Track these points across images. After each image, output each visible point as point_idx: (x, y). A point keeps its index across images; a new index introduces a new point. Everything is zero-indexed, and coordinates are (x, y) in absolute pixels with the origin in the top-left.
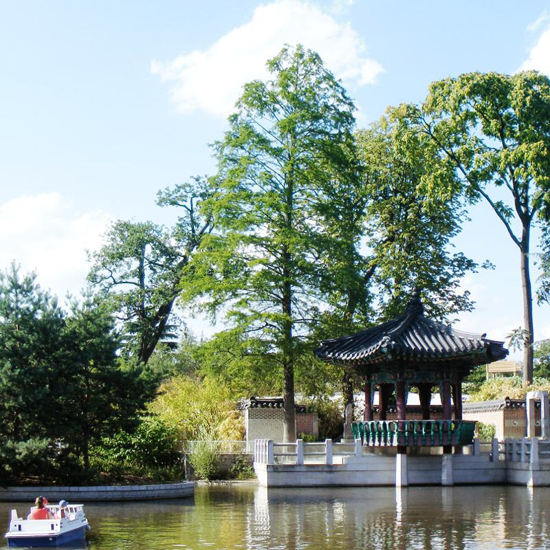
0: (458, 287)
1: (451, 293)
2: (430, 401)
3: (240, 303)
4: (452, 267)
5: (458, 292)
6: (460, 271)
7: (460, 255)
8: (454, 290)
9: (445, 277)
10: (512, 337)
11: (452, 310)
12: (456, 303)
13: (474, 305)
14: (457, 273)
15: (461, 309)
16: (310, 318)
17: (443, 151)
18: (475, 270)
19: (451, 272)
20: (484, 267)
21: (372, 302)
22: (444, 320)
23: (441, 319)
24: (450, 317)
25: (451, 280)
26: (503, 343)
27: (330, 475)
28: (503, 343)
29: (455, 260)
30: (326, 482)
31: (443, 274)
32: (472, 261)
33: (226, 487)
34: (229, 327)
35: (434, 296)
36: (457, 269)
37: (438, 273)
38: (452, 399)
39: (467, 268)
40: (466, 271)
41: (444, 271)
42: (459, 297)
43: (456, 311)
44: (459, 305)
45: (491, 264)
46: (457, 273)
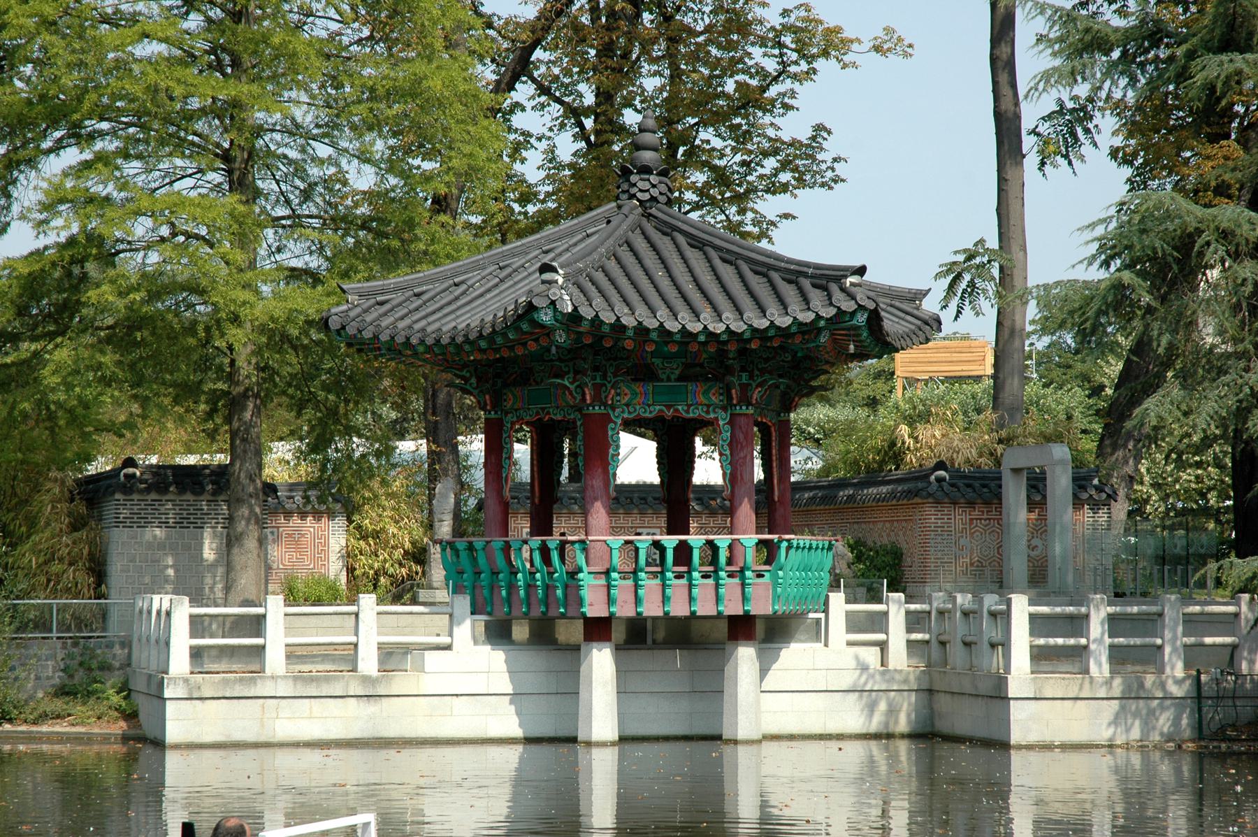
0: (790, 113)
1: (771, 132)
2: (691, 474)
3: (86, 165)
4: (776, 52)
5: (793, 127)
6: (803, 63)
7: (803, 14)
8: (777, 121)
9: (754, 82)
10: (954, 273)
11: (775, 188)
12: (785, 165)
13: (832, 146)
14: (793, 69)
15: (801, 183)
16: (314, 211)
17: (317, 21)
18: (846, 58)
19: (771, 66)
20: (877, 49)
21: (523, 161)
22: (750, 215)
23: (742, 212)
24: (769, 206)
25: (773, 91)
26: (925, 293)
27: (372, 708)
28: (925, 293)
29: (786, 28)
30: (355, 732)
31: (745, 71)
32: (838, 30)
33: (518, 52)
34: (51, 239)
35: (717, 143)
36: (794, 56)
37: (732, 67)
38: (758, 462)
39: (825, 54)
40: (820, 64)
41: (750, 63)
42: (794, 143)
43: (784, 188)
44: (795, 170)
45: (900, 39)
46: (793, 69)
